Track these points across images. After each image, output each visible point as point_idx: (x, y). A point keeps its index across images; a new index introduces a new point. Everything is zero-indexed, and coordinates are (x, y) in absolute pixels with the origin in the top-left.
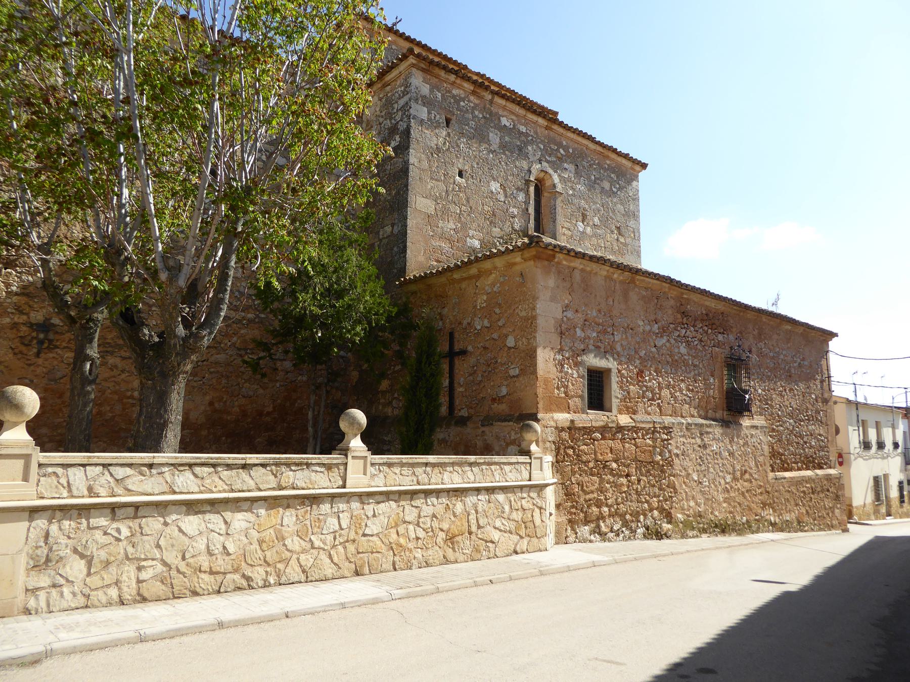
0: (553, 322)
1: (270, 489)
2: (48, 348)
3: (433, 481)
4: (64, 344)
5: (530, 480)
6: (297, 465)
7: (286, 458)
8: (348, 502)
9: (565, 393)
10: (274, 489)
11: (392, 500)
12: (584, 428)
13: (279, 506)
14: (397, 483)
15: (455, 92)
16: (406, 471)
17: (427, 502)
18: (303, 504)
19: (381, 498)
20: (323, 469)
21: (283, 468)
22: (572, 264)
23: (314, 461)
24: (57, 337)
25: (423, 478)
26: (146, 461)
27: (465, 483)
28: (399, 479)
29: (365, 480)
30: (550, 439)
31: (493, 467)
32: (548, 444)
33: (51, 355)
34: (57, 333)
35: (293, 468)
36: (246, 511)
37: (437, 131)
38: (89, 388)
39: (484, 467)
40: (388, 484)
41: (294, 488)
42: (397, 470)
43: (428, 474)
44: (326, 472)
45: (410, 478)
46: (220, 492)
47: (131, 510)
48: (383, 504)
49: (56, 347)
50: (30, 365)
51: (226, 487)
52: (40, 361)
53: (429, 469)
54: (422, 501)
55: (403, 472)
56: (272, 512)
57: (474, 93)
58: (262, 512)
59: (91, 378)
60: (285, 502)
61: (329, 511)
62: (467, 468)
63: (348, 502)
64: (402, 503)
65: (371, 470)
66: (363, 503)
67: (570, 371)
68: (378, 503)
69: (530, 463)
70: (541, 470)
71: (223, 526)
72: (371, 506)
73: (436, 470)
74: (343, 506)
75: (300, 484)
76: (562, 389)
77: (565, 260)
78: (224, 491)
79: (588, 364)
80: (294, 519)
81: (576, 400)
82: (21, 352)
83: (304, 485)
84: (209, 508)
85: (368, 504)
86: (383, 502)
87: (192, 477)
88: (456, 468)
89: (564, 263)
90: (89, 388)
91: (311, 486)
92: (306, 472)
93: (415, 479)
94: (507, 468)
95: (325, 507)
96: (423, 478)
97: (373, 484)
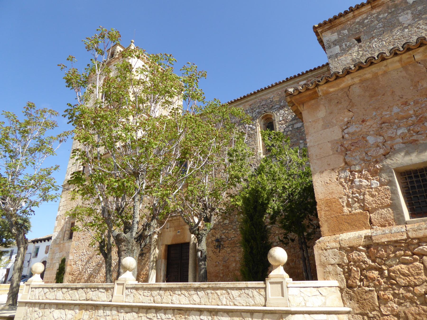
0: (329, 145)
1: (83, 300)
2: (222, 248)
3: (164, 301)
4: (227, 246)
5: (265, 306)
6: (94, 288)
7: (90, 285)
8: (111, 310)
9: (363, 208)
10: (84, 300)
11: (134, 312)
12: (396, 242)
13: (84, 309)
14: (141, 301)
15: (357, 20)
16: (147, 293)
17: (157, 316)
18: (92, 309)
19: (127, 310)
20: (104, 291)
21: (89, 290)
22: (342, 85)
23: (100, 286)
24: (224, 243)
25: (158, 298)
26: (51, 286)
27: (191, 304)
28: (142, 298)
29: (124, 298)
30: (333, 262)
31: (219, 292)
32: (330, 268)
33: (223, 251)
34: (224, 241)
35: (92, 290)
36: (72, 310)
37: (350, 52)
38: (201, 263)
39: (209, 291)
40: (135, 301)
41: (92, 300)
42: (141, 292)
43: (161, 296)
44: (106, 292)
45: (149, 298)
46: (68, 300)
47: (43, 305)
48: (129, 314)
49: (225, 247)
50: (217, 256)
51: (70, 298)
52: (220, 254)
53: (162, 292)
54: (154, 315)
55: (145, 294)
56: (80, 311)
57: (373, 8)
58: (77, 311)
59: (201, 259)
60: (85, 307)
61: (102, 314)
62: (193, 292)
63: (111, 310)
64: (141, 315)
65: (126, 291)
66: (118, 312)
67: (365, 182)
68: (127, 313)
69: (265, 288)
70: (283, 296)
71: (65, 316)
72: (123, 314)
73: (168, 293)
74: (108, 312)
75: (94, 298)
76: (356, 205)
77: (331, 87)
78: (69, 300)
79: (395, 166)
80: (88, 316)
81: (384, 211)
82: (215, 252)
83: (95, 299)
84: (61, 307)
85: (121, 313)
86: (129, 312)
87: (61, 293)
88: (183, 292)
89: (332, 90)
90: (201, 263)
91: (98, 300)
92: (97, 292)
93: (152, 299)
94: (235, 293)
95: (101, 312)
96: (158, 298)
97: (127, 301)
